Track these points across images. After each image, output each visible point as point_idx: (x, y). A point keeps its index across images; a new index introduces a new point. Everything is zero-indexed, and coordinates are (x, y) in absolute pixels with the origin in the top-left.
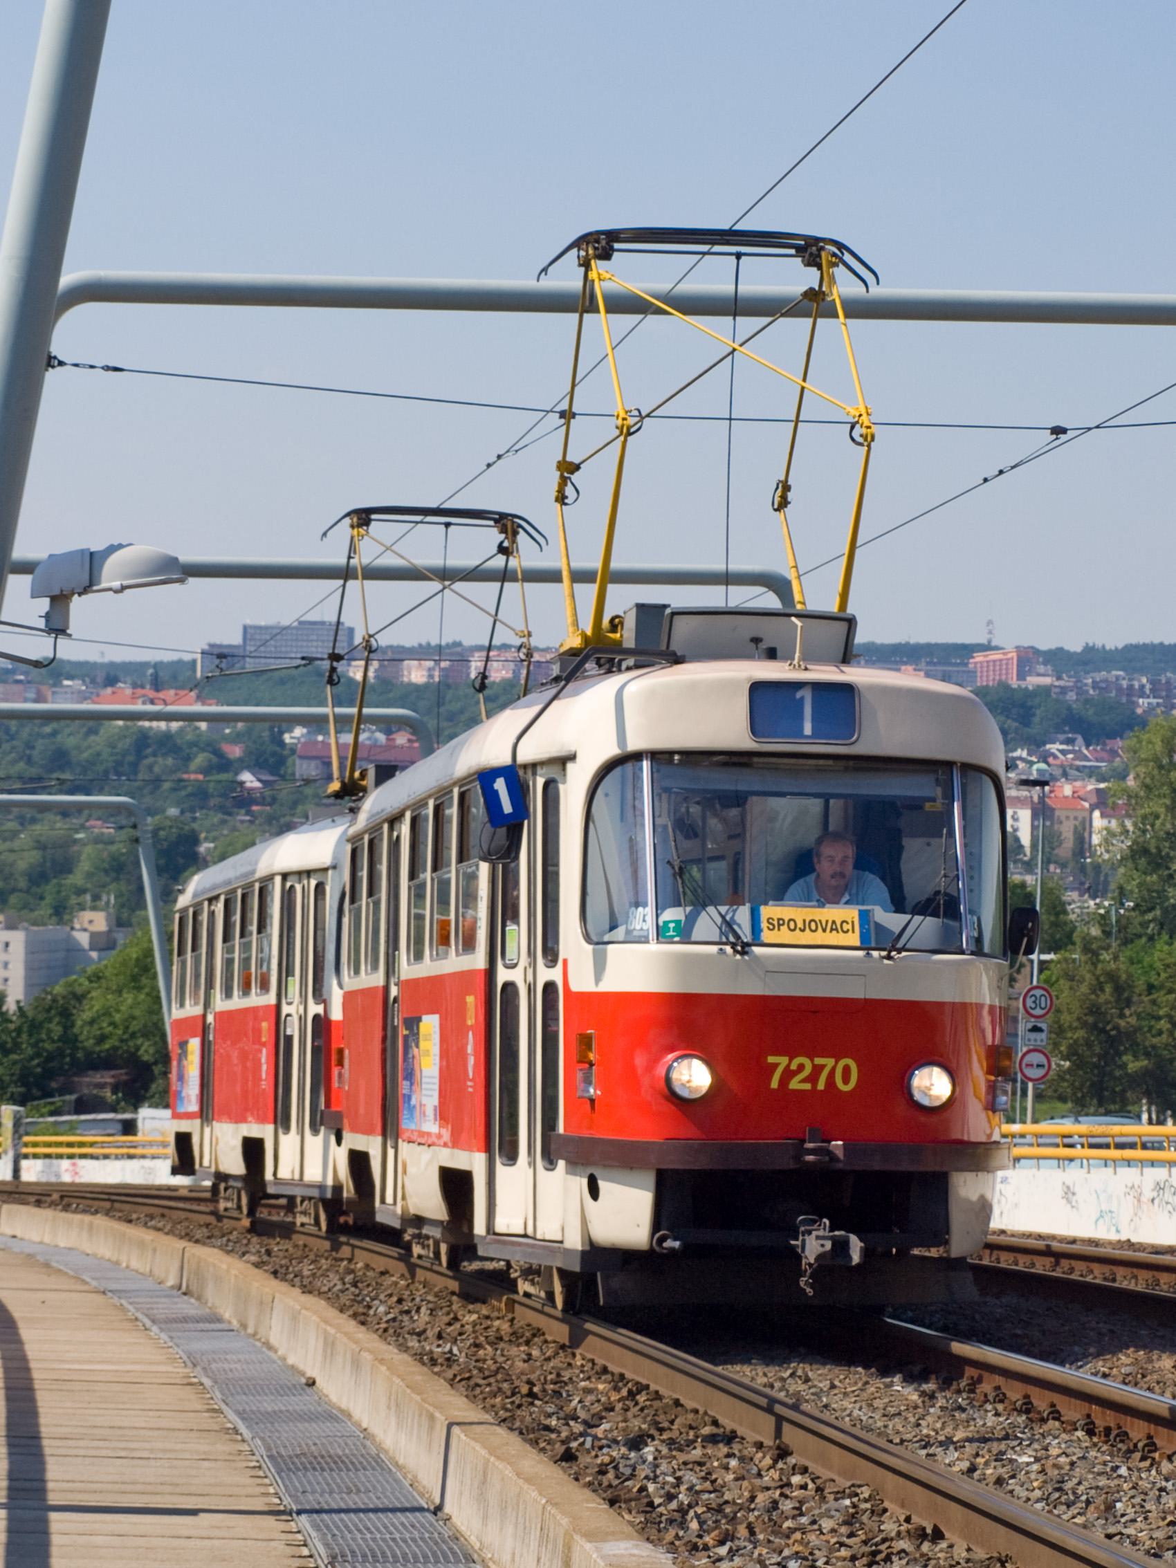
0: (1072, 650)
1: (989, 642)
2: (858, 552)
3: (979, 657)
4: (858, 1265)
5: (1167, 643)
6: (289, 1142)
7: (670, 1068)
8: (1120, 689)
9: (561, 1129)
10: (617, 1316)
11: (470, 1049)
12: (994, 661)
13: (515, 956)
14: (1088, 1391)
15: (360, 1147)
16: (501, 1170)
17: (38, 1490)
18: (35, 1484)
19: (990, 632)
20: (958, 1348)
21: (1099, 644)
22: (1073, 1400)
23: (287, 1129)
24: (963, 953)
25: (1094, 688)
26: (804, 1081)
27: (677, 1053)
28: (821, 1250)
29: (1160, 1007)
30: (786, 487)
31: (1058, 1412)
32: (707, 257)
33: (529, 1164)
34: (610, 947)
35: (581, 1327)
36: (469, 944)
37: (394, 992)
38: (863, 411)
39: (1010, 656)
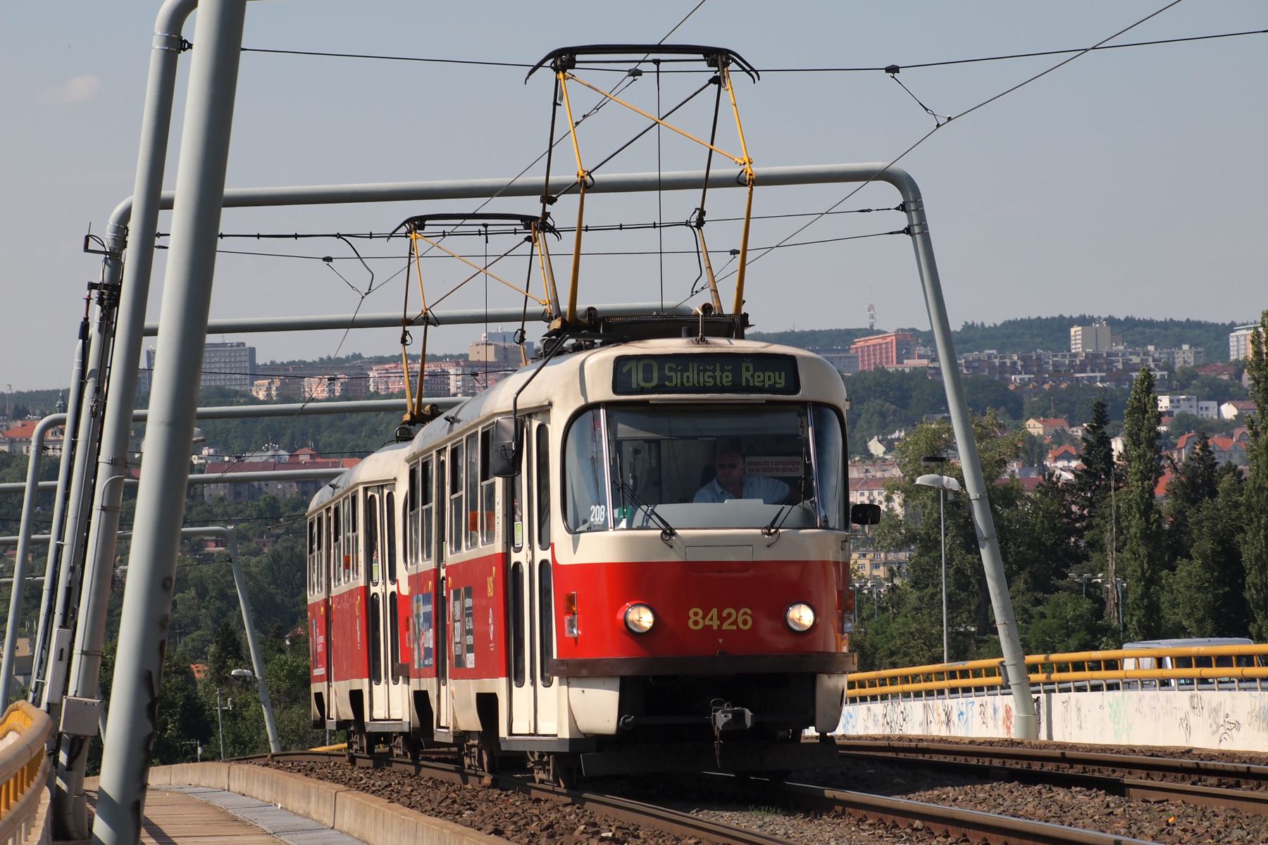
1: (872, 326)
2: (747, 267)
3: (860, 343)
4: (751, 727)
5: (1044, 317)
7: (626, 614)
8: (992, 367)
12: (874, 346)
13: (520, 542)
19: (872, 317)
21: (978, 322)
24: (817, 528)
25: (966, 367)
26: (730, 624)
27: (635, 602)
28: (725, 720)
34: (582, 535)
36: (490, 537)
37: (443, 573)
38: (747, 160)
39: (889, 339)
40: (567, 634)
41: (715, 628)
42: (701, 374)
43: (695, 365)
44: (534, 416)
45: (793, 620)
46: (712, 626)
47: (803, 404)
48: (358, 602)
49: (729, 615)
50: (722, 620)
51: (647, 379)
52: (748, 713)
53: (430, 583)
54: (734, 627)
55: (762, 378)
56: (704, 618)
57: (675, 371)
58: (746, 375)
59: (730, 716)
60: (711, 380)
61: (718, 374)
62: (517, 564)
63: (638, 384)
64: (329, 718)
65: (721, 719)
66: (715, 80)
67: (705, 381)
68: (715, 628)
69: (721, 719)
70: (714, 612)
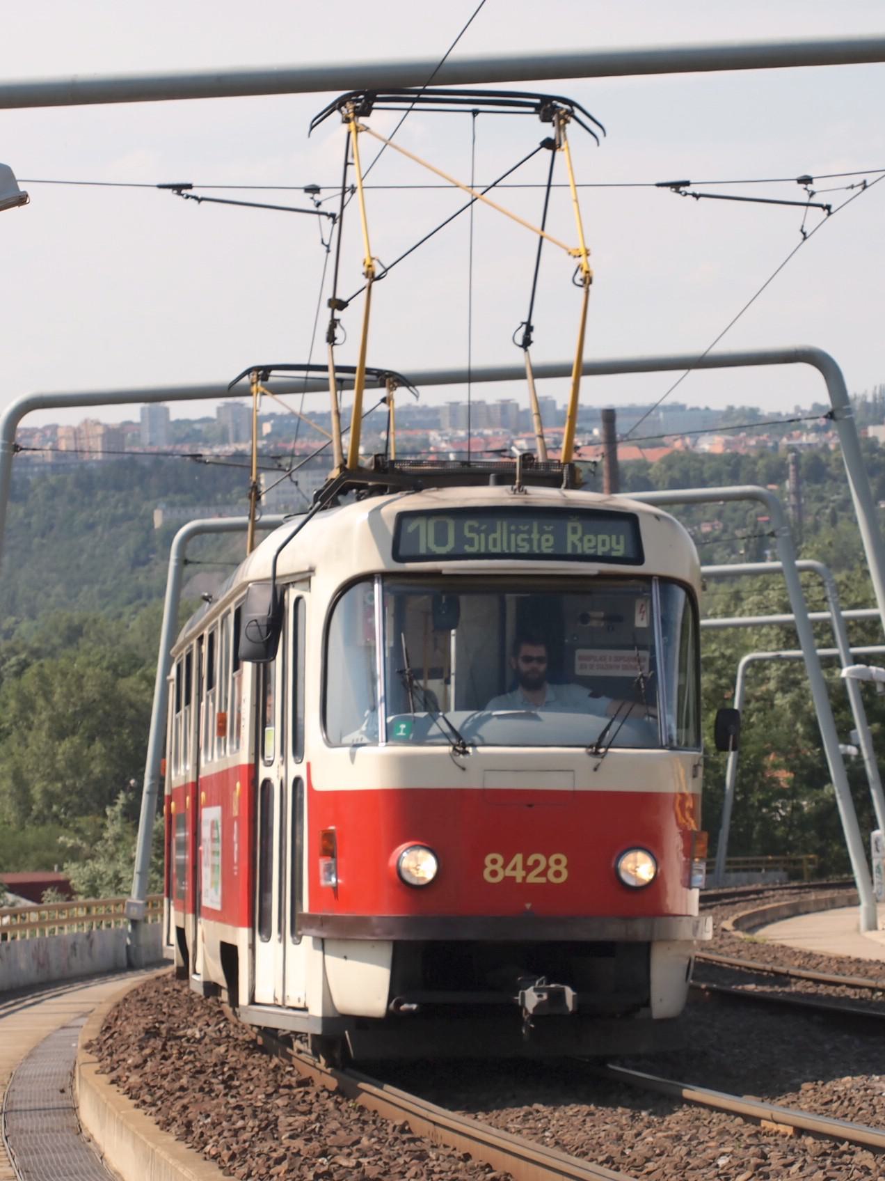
4: (573, 1013)
6: (269, 951)
9: (306, 908)
10: (385, 1073)
11: (235, 838)
15: (229, 941)
16: (259, 944)
23: (267, 936)
26: (539, 875)
27: (426, 845)
30: (529, 329)
32: (411, 112)
33: (280, 940)
38: (583, 251)
40: (323, 883)
41: (519, 880)
42: (513, 536)
43: (505, 524)
44: (291, 586)
45: (627, 872)
46: (514, 878)
47: (647, 578)
48: (237, 793)
49: (537, 863)
50: (528, 869)
51: (441, 539)
52: (569, 993)
53: (238, 785)
54: (542, 880)
55: (593, 544)
56: (504, 867)
57: (478, 531)
58: (572, 538)
59: (545, 997)
60: (525, 544)
61: (535, 536)
62: (267, 782)
63: (428, 548)
64: (195, 972)
65: (531, 999)
66: (550, 144)
67: (517, 546)
68: (519, 880)
69: (531, 999)
70: (518, 858)
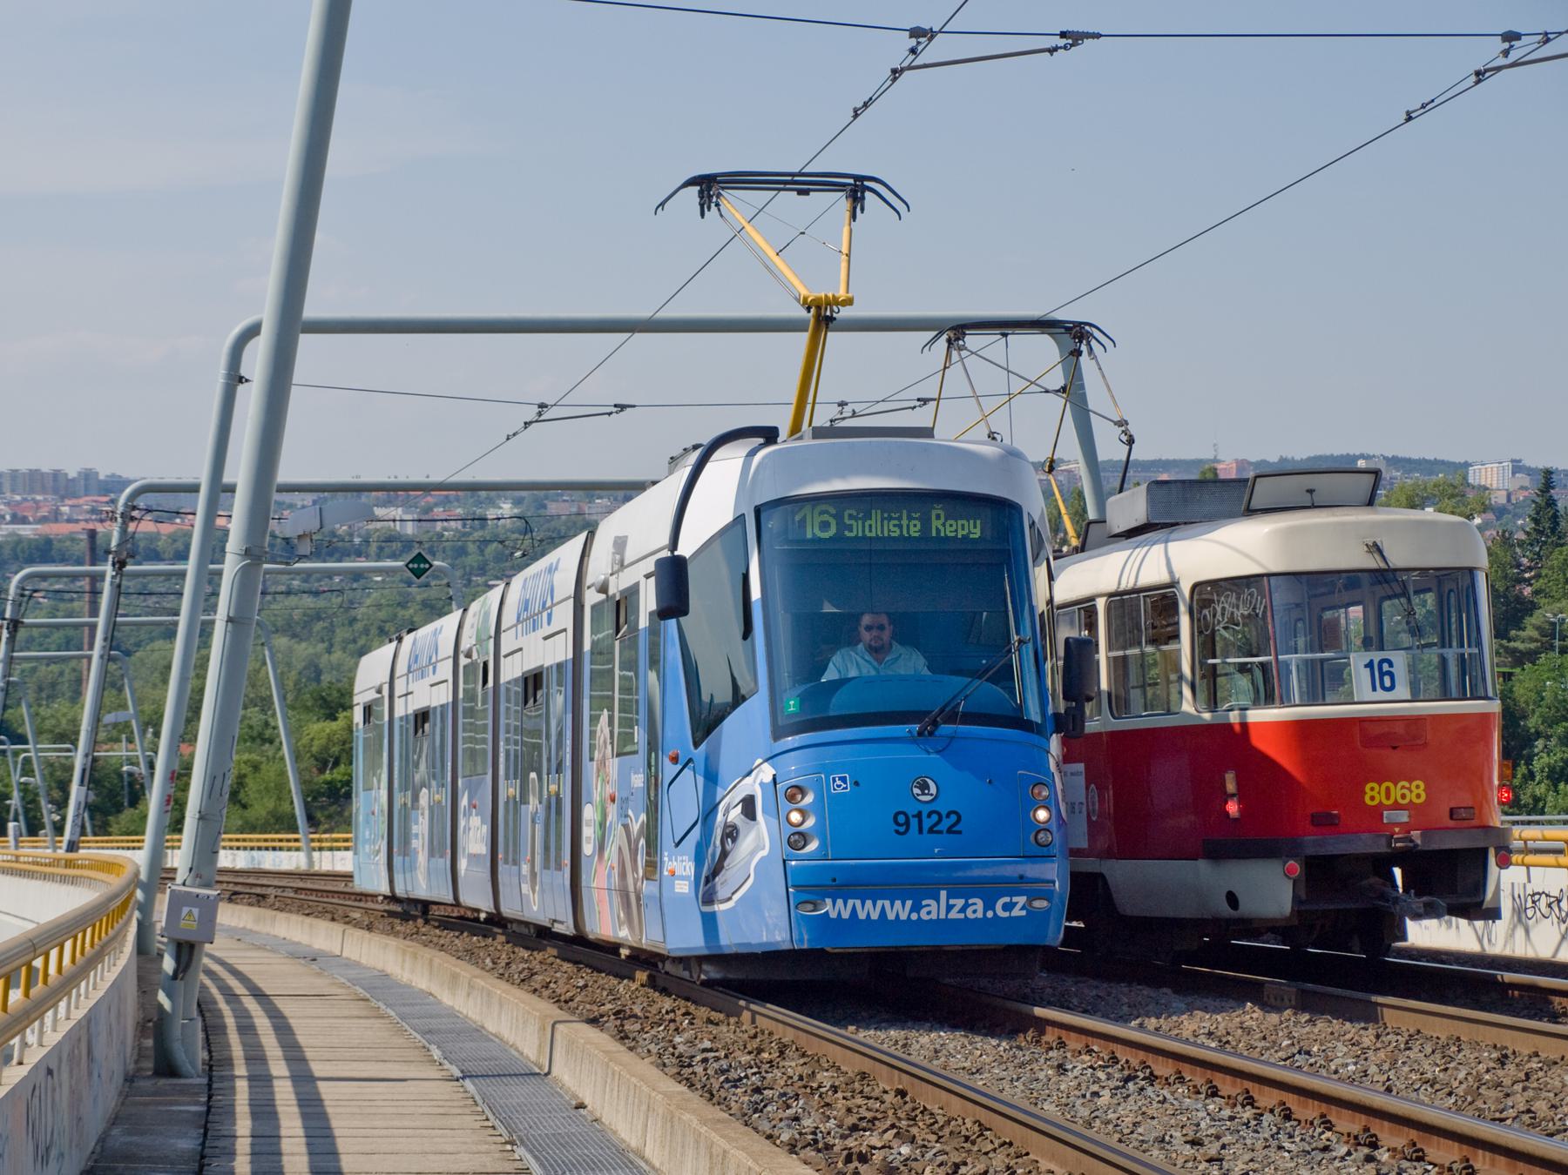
0: (1271, 461)
14: (1510, 1145)
17: (270, 1113)
18: (268, 1109)
20: (1039, 1011)
22: (1357, 1115)
29: (1563, 799)
31: (1252, 1097)
35: (737, 1004)
